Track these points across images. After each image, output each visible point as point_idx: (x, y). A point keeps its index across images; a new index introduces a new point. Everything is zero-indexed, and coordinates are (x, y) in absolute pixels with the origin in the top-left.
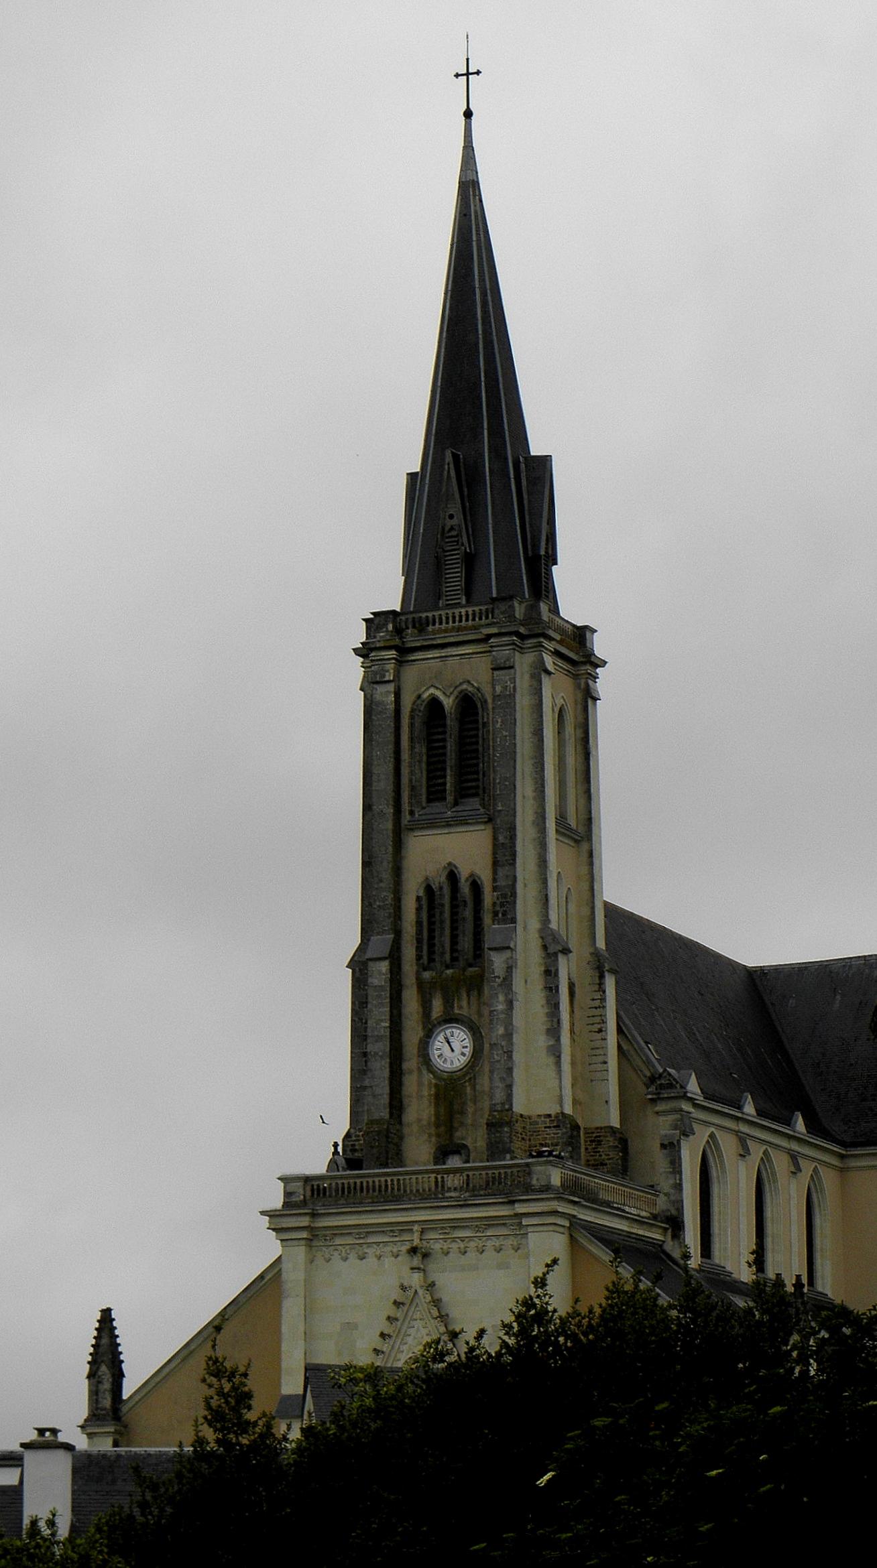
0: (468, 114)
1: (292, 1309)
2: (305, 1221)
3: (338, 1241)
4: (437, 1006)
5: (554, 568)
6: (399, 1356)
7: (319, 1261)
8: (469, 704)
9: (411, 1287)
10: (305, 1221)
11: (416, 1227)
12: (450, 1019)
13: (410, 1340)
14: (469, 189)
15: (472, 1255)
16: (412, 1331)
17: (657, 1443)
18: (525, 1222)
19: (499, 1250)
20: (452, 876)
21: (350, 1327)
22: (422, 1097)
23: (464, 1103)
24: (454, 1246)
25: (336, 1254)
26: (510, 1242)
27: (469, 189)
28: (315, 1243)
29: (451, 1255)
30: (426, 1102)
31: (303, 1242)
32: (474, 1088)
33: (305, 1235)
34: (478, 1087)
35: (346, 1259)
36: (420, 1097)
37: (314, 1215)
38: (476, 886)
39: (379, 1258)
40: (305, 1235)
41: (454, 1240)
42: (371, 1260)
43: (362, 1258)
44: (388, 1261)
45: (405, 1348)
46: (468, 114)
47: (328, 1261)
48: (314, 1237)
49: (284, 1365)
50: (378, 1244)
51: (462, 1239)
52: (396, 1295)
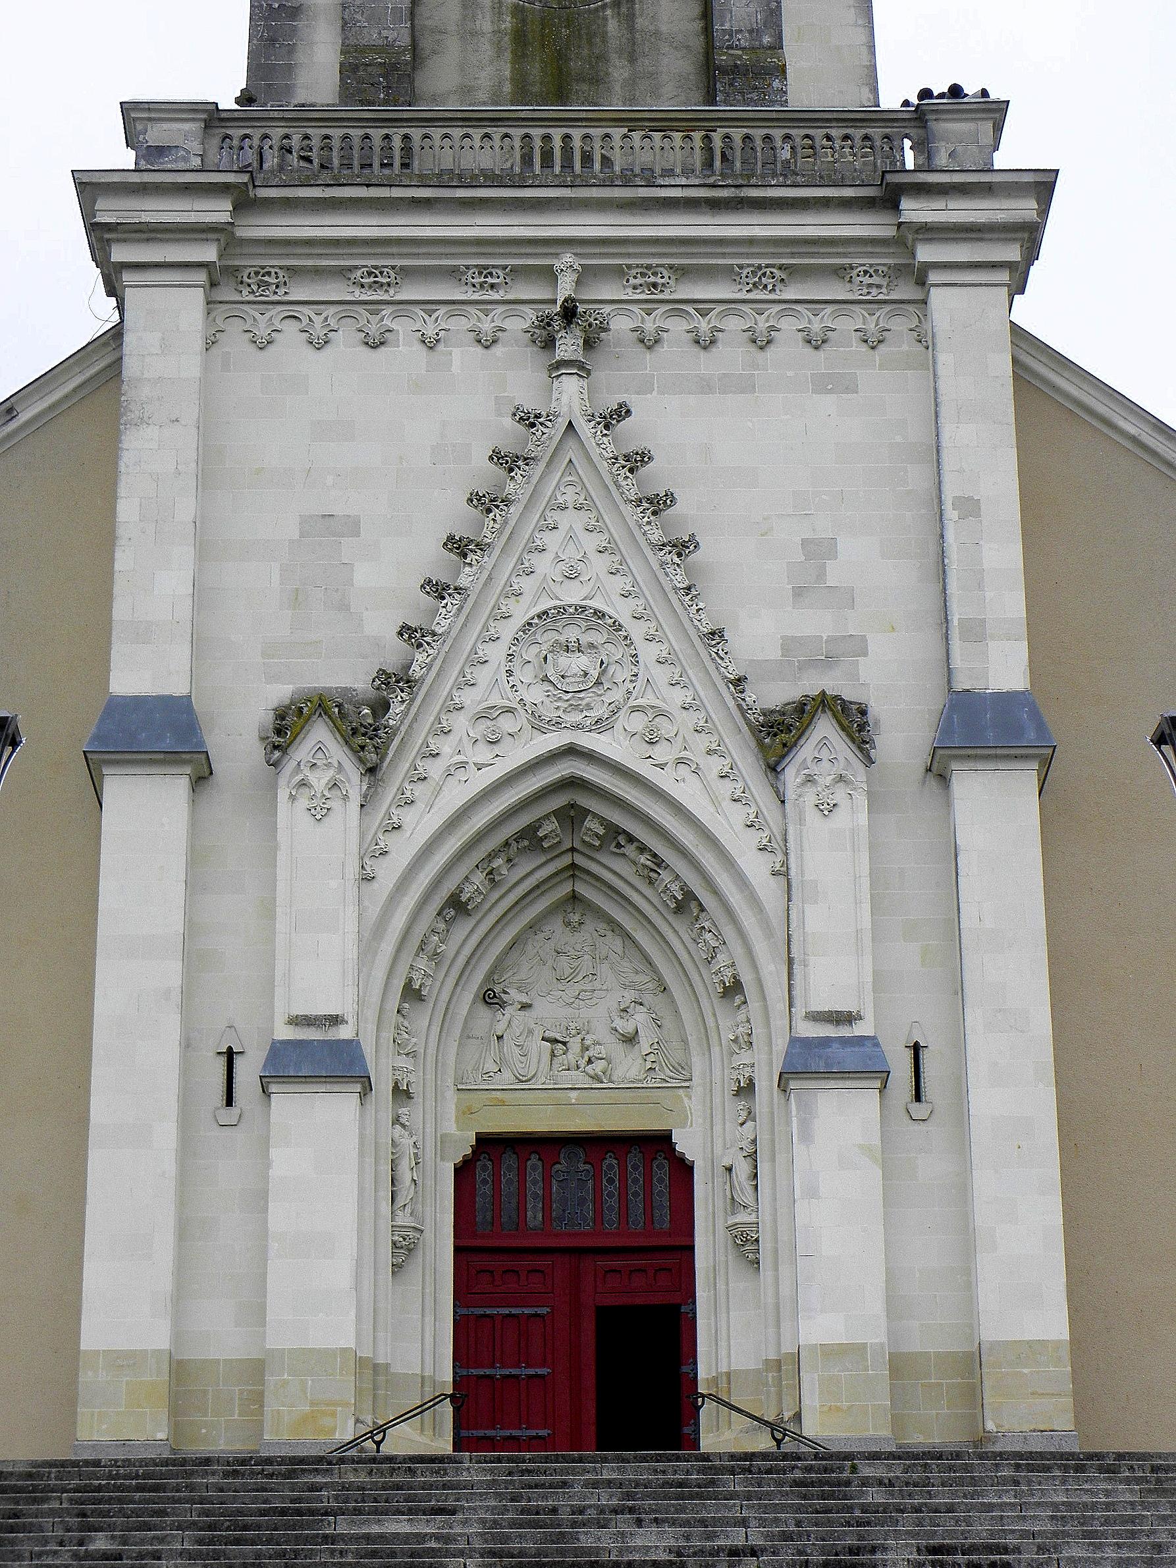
1: (153, 458)
2: (218, 211)
3: (299, 292)
6: (511, 606)
7: (235, 341)
9: (551, 417)
10: (218, 211)
13: (543, 564)
15: (732, 354)
16: (551, 540)
17: (104, 1427)
18: (925, 253)
19: (816, 343)
21: (331, 527)
22: (474, 34)
23: (603, 58)
25: (291, 327)
26: (847, 324)
28: (226, 293)
29: (663, 349)
30: (486, 48)
31: (201, 277)
32: (631, 18)
33: (209, 253)
34: (640, 22)
35: (320, 344)
36: (469, 35)
37: (244, 203)
39: (430, 344)
40: (209, 253)
41: (677, 307)
42: (405, 352)
44: (461, 357)
45: (527, 584)
47: (263, 345)
48: (232, 276)
49: (120, 610)
51: (703, 307)
52: (508, 435)
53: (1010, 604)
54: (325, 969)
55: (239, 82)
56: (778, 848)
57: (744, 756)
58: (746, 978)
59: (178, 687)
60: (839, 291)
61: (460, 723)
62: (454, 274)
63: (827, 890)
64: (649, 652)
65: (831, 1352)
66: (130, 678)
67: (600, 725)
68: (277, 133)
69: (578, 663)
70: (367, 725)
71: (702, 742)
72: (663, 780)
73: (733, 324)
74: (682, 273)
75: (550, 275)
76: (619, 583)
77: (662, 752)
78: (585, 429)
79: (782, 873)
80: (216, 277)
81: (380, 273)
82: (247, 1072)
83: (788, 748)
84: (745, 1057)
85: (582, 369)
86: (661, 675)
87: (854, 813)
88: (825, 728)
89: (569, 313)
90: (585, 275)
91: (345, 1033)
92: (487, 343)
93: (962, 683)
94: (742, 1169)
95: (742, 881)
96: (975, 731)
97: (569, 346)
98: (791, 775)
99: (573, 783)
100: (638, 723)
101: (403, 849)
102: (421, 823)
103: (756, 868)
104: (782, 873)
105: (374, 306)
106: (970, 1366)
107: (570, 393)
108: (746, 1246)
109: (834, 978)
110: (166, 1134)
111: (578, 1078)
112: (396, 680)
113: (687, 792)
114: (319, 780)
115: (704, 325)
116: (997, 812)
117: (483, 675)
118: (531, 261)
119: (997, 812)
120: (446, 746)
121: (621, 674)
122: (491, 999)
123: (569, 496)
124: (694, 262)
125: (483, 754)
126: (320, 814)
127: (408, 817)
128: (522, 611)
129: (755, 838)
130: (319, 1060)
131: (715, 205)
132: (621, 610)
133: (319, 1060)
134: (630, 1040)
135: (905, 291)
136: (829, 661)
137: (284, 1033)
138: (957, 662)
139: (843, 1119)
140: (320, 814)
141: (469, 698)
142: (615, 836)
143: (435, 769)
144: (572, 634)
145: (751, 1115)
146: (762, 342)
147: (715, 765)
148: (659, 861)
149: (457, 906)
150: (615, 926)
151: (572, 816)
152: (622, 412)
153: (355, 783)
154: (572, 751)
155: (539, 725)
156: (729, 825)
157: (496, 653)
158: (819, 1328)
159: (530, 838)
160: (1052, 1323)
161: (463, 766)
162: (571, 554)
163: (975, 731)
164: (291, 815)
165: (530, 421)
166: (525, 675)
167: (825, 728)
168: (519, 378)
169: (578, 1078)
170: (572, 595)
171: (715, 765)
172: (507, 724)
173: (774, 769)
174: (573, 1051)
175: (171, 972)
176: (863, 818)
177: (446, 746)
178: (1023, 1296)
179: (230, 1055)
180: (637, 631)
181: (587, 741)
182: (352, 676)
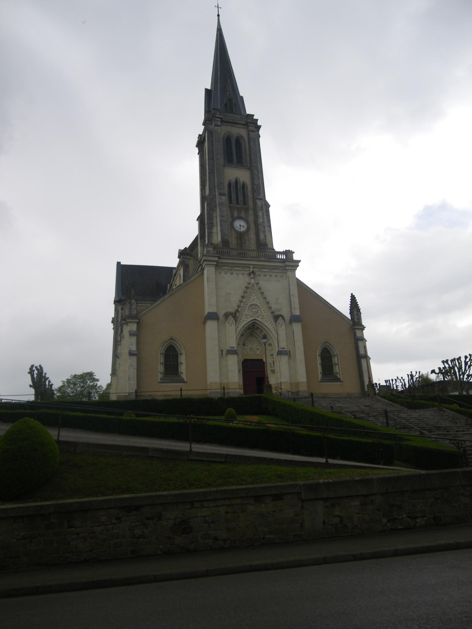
0: (218, 15)
2: (217, 259)
3: (224, 268)
4: (236, 214)
5: (201, 133)
8: (238, 140)
10: (217, 259)
11: (251, 266)
12: (240, 218)
14: (219, 31)
16: (252, 297)
18: (287, 268)
19: (276, 276)
20: (236, 182)
24: (262, 274)
27: (219, 31)
32: (248, 236)
35: (226, 274)
37: (219, 258)
38: (244, 186)
39: (237, 274)
40: (215, 263)
41: (262, 272)
43: (232, 274)
44: (241, 276)
46: (218, 15)
50: (237, 270)
51: (265, 272)
53: (297, 306)
54: (232, 342)
55: (189, 232)
56: (277, 330)
57: (272, 320)
58: (272, 343)
59: (216, 311)
60: (278, 271)
61: (244, 316)
62: (239, 267)
63: (280, 335)
64: (262, 309)
65: (285, 382)
66: (208, 310)
67: (258, 317)
68: (220, 250)
69: (255, 310)
70: (235, 315)
71: (268, 319)
72: (264, 323)
73: (268, 274)
74: (262, 268)
75: (250, 268)
76: (259, 302)
77: (264, 320)
78: (255, 285)
79: (277, 333)
80: (216, 266)
81: (234, 266)
82: (224, 353)
83: (277, 320)
84: (272, 352)
85: (254, 278)
86: (263, 312)
87: (284, 327)
88: (280, 318)
89: (253, 272)
90: (253, 268)
91: (235, 349)
92: (243, 274)
93: (293, 314)
94: (272, 363)
95: (272, 333)
96: (294, 319)
97: (252, 276)
98: (277, 323)
99: (254, 323)
100: (261, 317)
101: (239, 329)
102: (241, 326)
103: (274, 332)
104: (277, 333)
105: (231, 270)
106: (298, 384)
107: (253, 281)
108: (273, 372)
109: (283, 344)
110: (218, 360)
111: (253, 353)
112: (237, 311)
113: (267, 324)
114: (231, 322)
115: (265, 274)
116: (297, 328)
117: (246, 311)
118: (248, 266)
119: (297, 328)
120: (242, 318)
121: (259, 311)
122: (244, 345)
123: (253, 292)
124: (264, 267)
125: (246, 319)
126: (231, 325)
127: (239, 326)
128: (249, 304)
129: (274, 329)
130: (232, 352)
131: (266, 261)
132: (259, 305)
133: (232, 352)
134: (258, 349)
135: (284, 271)
136: (279, 311)
137: (229, 349)
138: (293, 311)
139: (284, 359)
140: (231, 325)
141: (244, 313)
142: (258, 328)
143: (241, 321)
144: (254, 307)
145: (273, 358)
146: (271, 276)
147: (269, 322)
148: (262, 331)
149: (242, 335)
150: (257, 338)
151: (253, 326)
152: (258, 283)
153: (234, 322)
154: (255, 319)
155: (251, 317)
156: (271, 328)
157: (247, 308)
158: (283, 380)
159: (249, 328)
160: (305, 380)
161: (245, 321)
162: (254, 299)
163: (294, 319)
164: (227, 325)
165: (249, 284)
166: (249, 311)
167: (280, 318)
168: (247, 279)
169: (253, 353)
170: (254, 303)
171: (269, 322)
172: (248, 316)
173: (276, 322)
174: (254, 351)
175: (217, 342)
176: (284, 328)
177: (242, 318)
178: (302, 377)
179: (222, 351)
180: (261, 307)
181: (256, 318)
182: (233, 311)
